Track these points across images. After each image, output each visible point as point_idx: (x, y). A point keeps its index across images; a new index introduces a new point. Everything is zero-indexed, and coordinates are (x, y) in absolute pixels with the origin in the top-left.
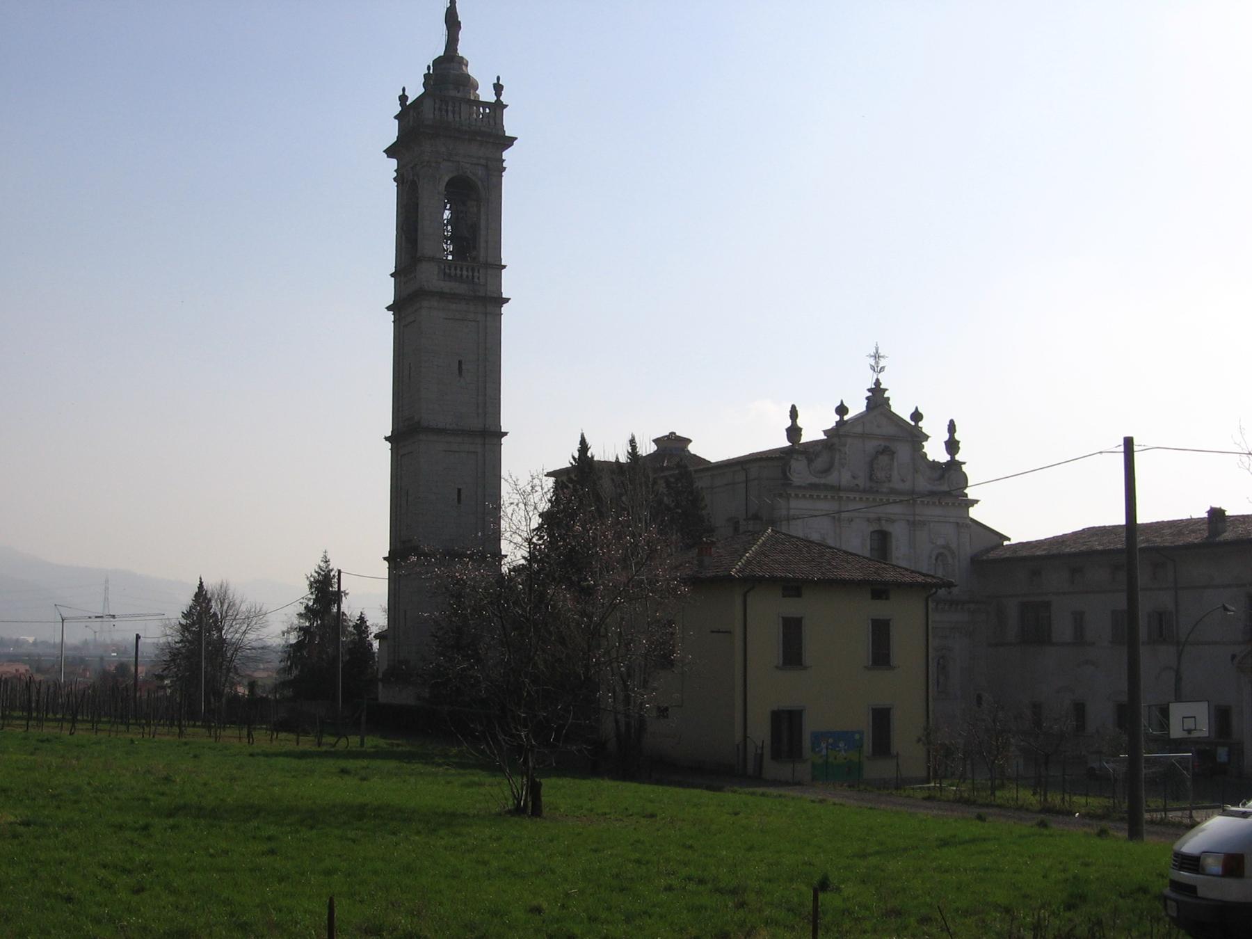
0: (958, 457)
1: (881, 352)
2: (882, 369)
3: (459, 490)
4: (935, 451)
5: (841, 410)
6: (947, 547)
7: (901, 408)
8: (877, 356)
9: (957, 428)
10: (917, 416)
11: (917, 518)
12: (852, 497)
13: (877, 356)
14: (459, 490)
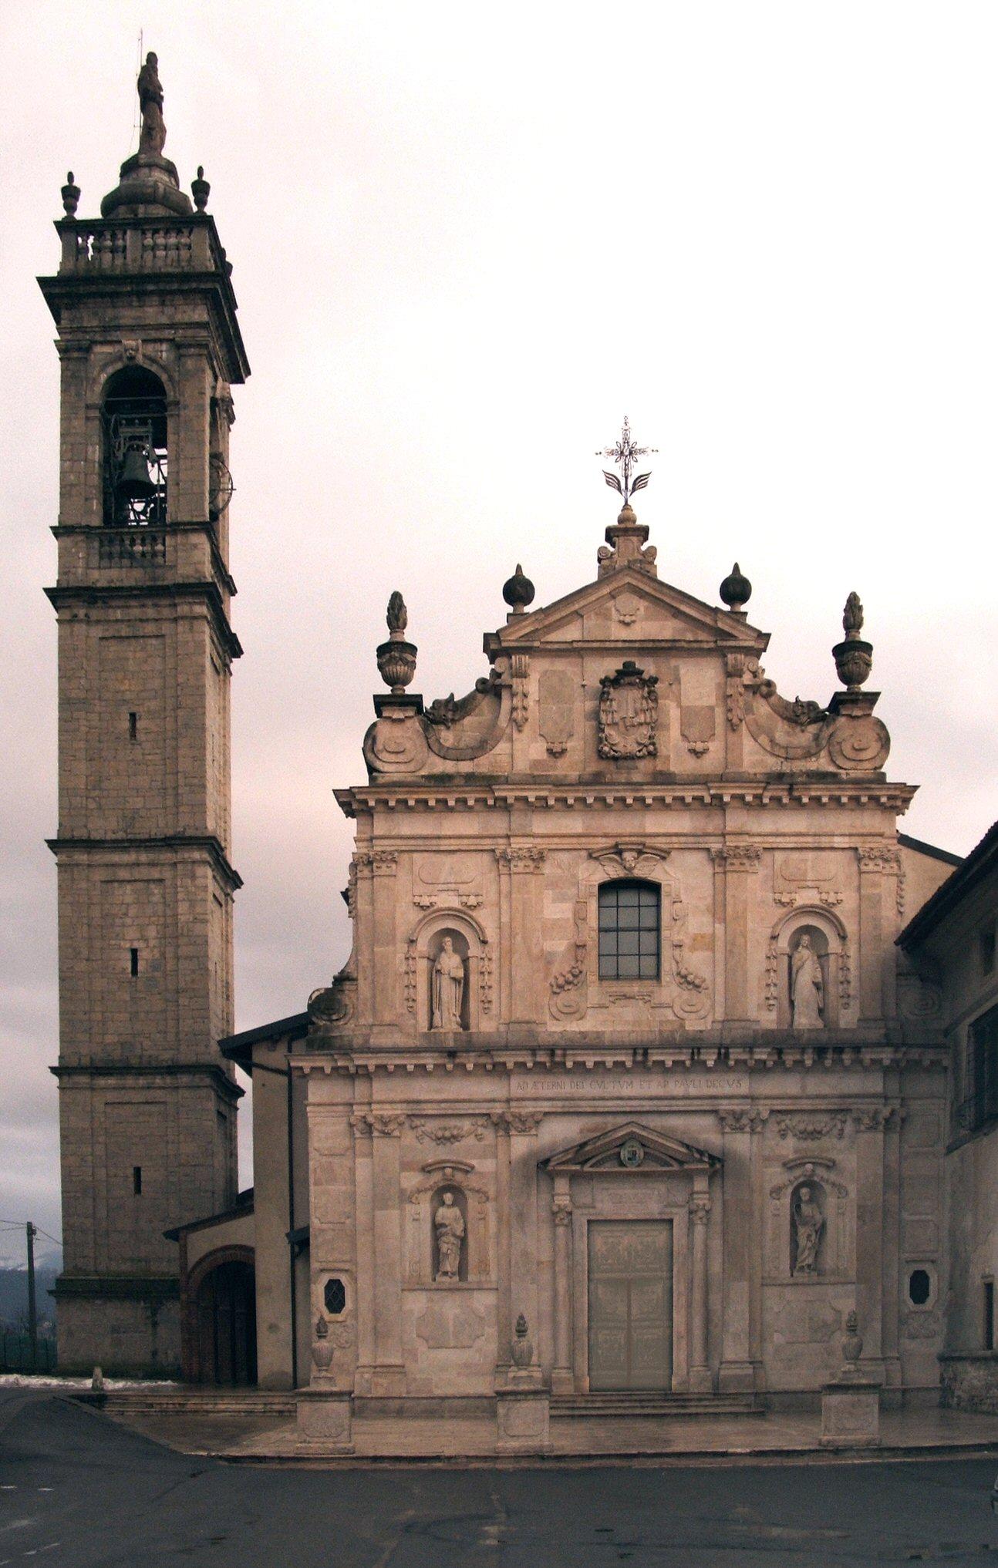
0: (866, 687)
1: (638, 439)
2: (641, 482)
3: (138, 1170)
4: (802, 671)
5: (518, 590)
6: (824, 911)
7: (690, 568)
8: (627, 452)
9: (866, 614)
10: (736, 589)
11: (731, 841)
12: (532, 796)
13: (627, 452)
14: (138, 1170)
